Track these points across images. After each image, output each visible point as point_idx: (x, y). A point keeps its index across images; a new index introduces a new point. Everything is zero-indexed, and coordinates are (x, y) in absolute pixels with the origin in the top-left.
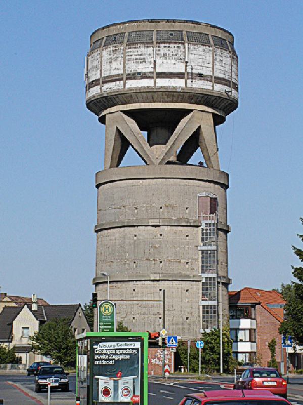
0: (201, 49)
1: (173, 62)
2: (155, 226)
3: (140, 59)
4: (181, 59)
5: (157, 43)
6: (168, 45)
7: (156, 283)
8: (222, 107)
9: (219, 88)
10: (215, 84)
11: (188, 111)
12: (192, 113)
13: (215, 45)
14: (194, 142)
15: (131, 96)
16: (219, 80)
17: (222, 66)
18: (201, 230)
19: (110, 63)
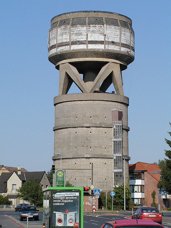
1: (98, 35)
2: (88, 127)
3: (79, 33)
4: (102, 33)
5: (89, 24)
7: (88, 159)
8: (125, 60)
9: (123, 50)
11: (107, 63)
13: (121, 25)
15: (74, 54)
16: (124, 45)
17: (125, 37)
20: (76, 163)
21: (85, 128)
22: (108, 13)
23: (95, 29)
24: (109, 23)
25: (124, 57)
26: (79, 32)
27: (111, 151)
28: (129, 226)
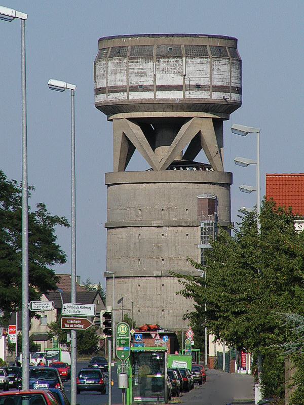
0: (198, 61)
1: (172, 75)
2: (158, 227)
3: (141, 73)
4: (179, 72)
5: (157, 58)
6: (167, 60)
7: (158, 279)
8: (220, 112)
9: (217, 96)
10: (213, 93)
11: (186, 120)
12: (192, 120)
13: (212, 55)
14: (197, 144)
15: (135, 106)
16: (217, 89)
17: (222, 72)
18: (200, 229)
19: (116, 74)
20: (139, 285)
21: (154, 228)
22: (191, 36)
24: (191, 55)
25: (218, 107)
26: (141, 70)
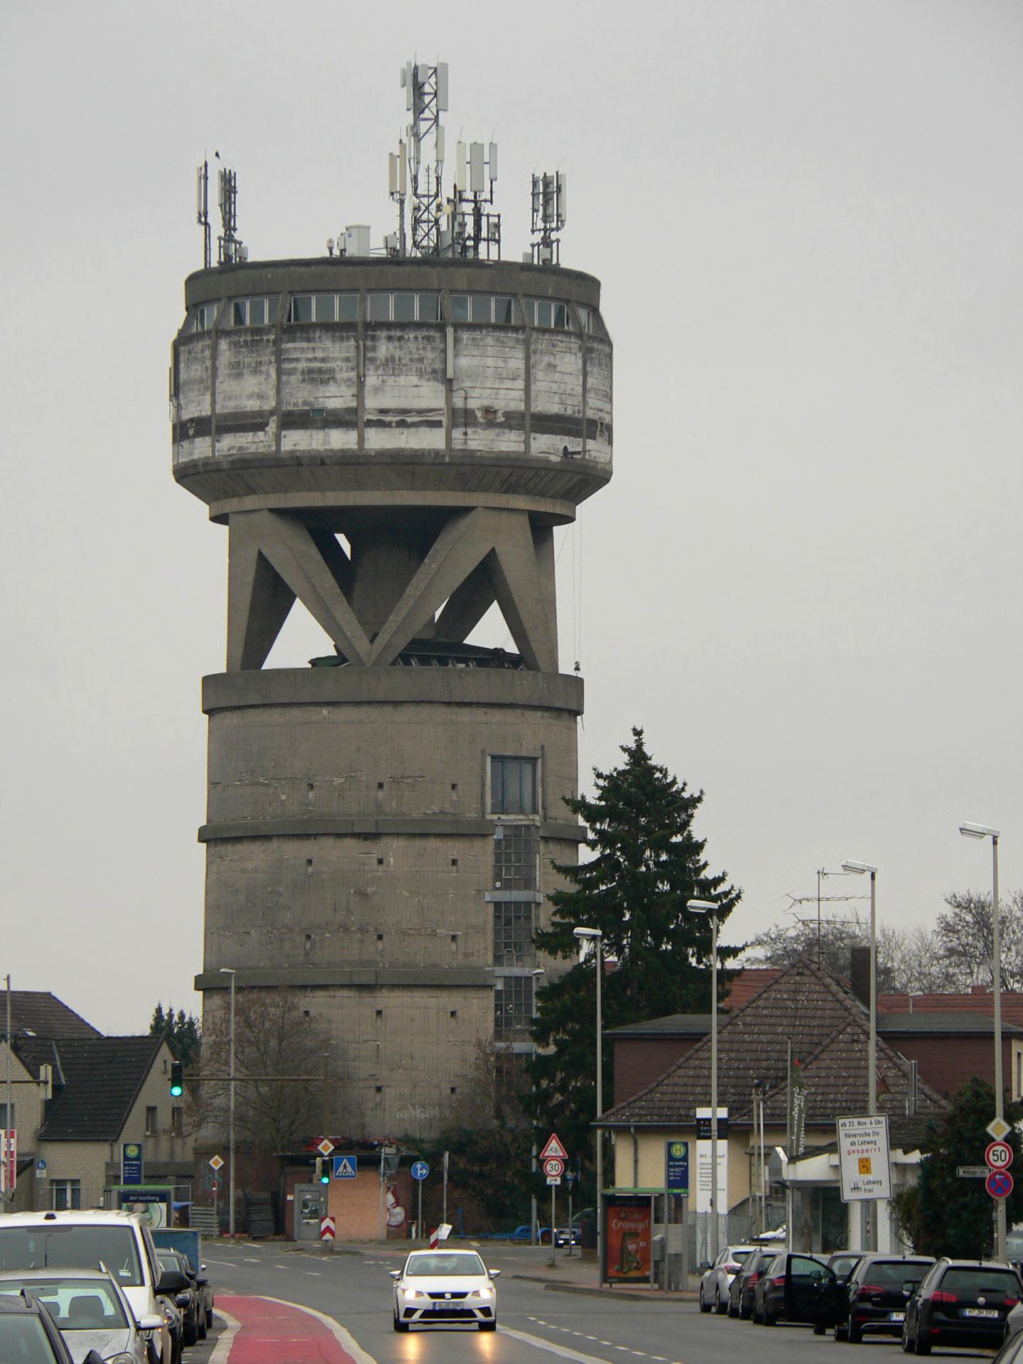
1: (414, 380)
3: (320, 371)
23: (397, 354)
27: (481, 949)
28: (631, 1039)
